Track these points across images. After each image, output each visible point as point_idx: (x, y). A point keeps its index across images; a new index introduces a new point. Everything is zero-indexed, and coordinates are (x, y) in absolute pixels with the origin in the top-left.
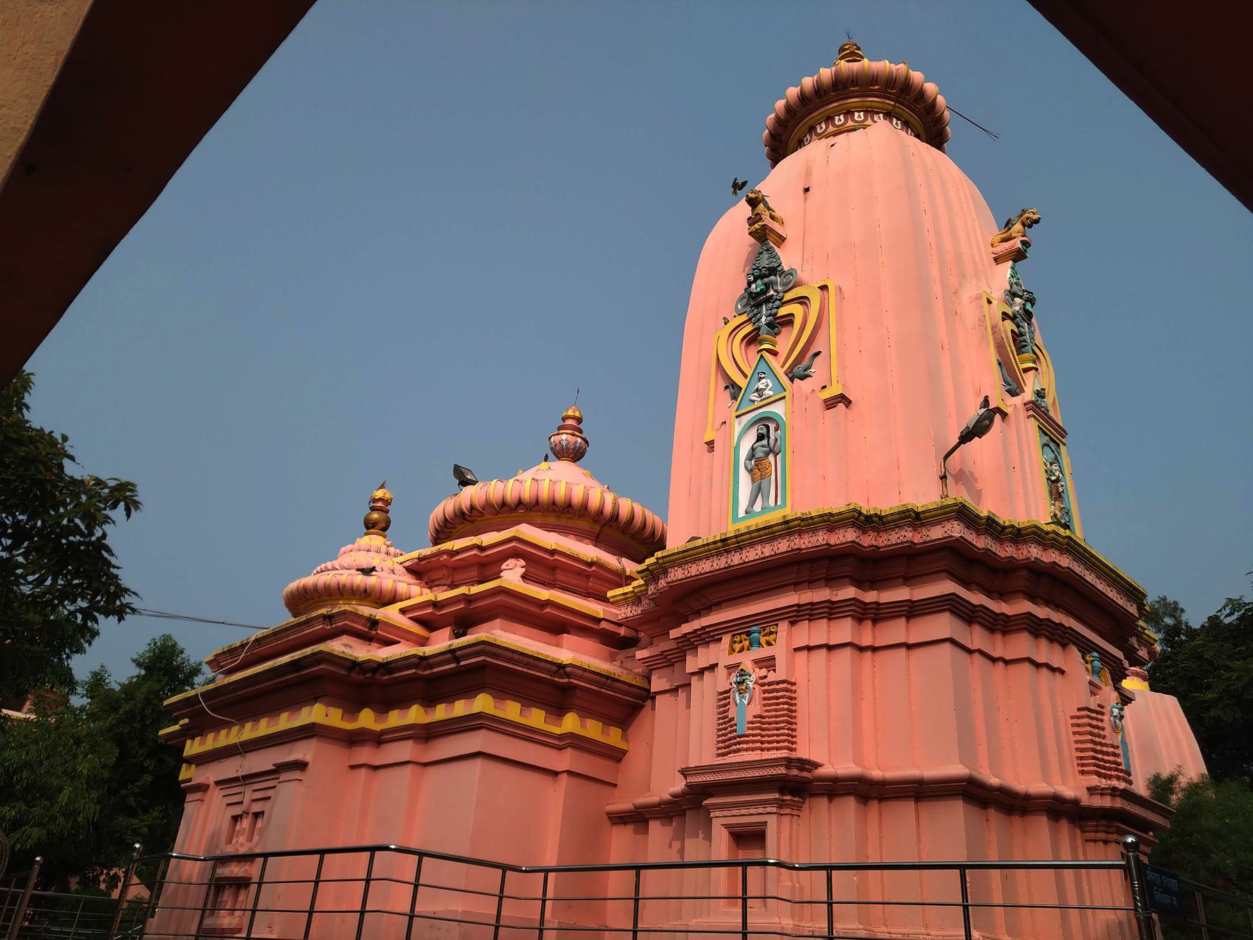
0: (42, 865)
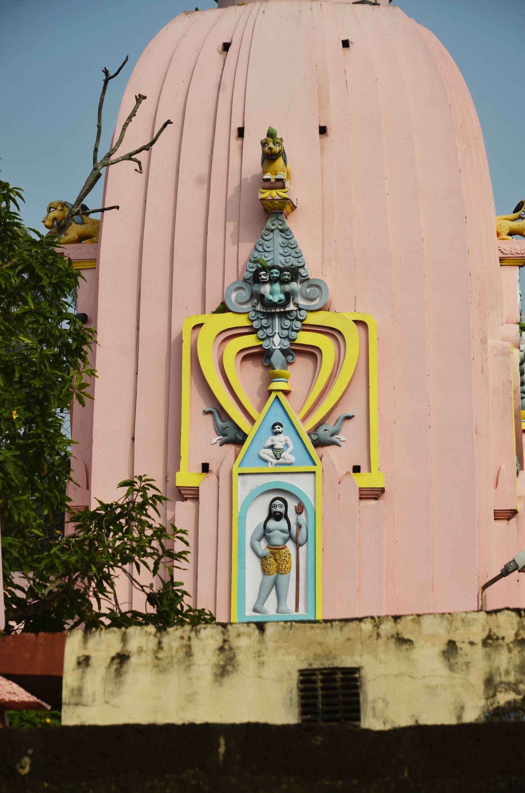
0: (37, 554)
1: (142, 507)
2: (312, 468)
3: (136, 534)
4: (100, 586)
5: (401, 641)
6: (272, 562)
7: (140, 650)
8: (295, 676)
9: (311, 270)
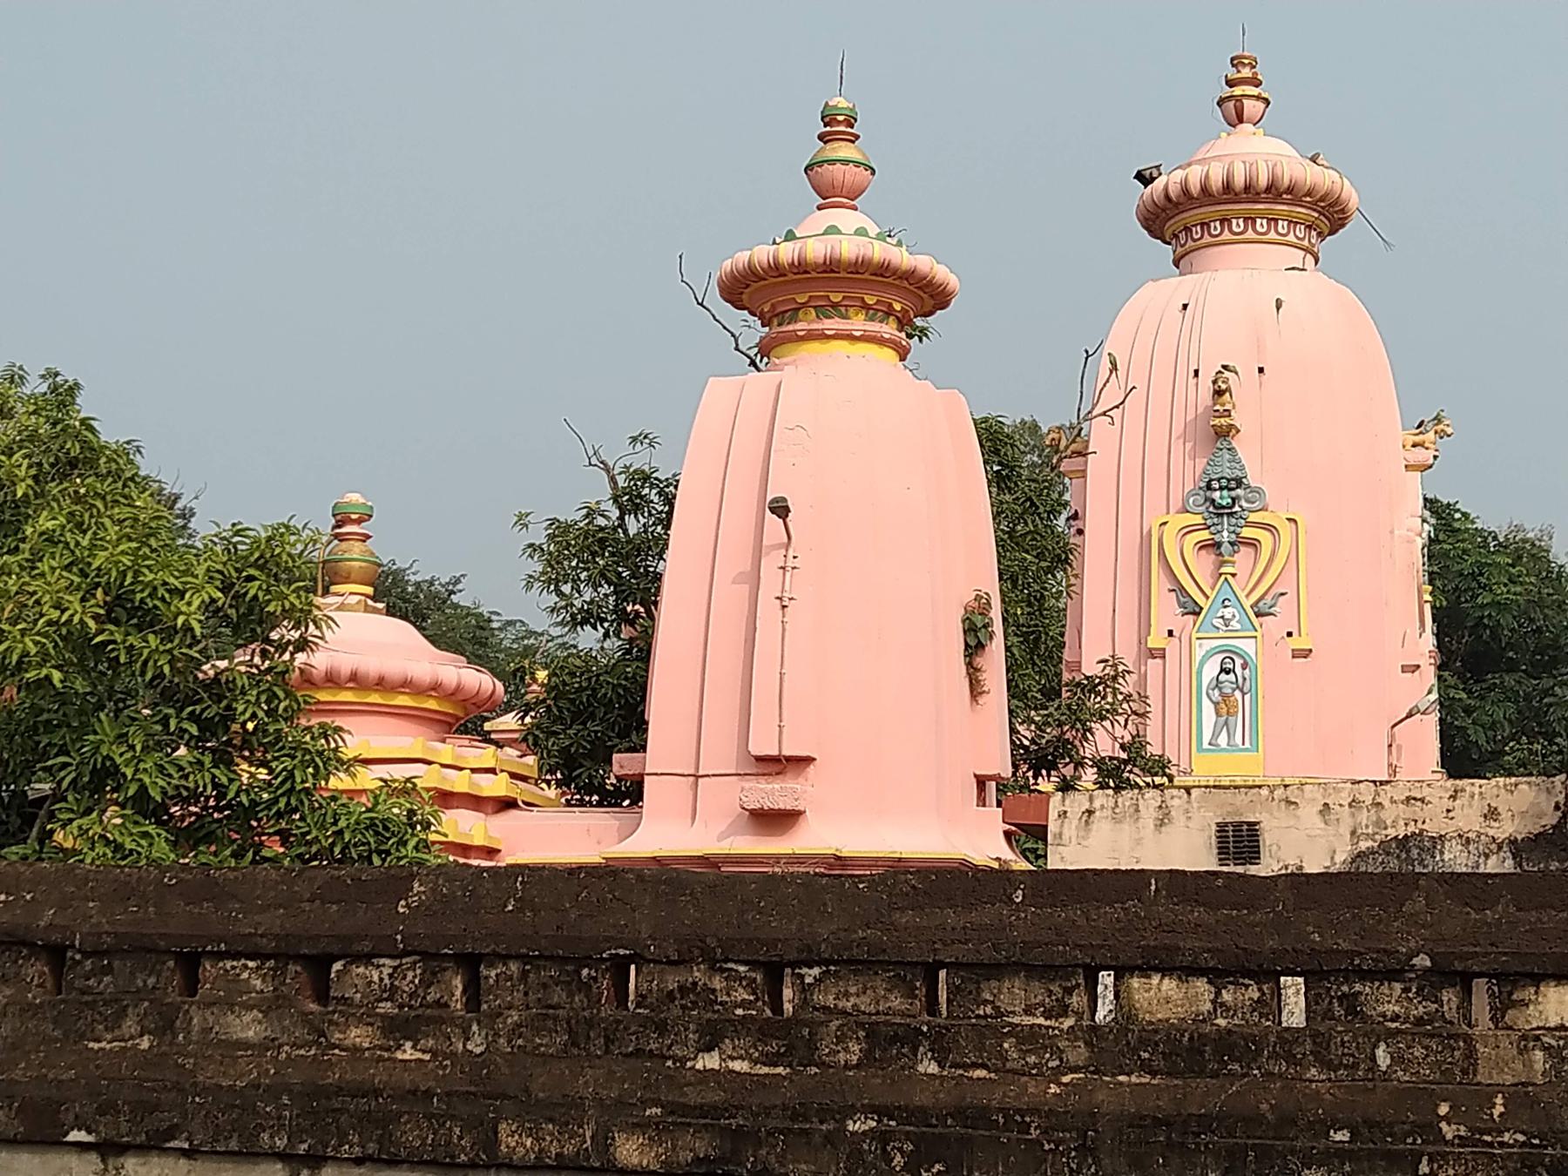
1: (1115, 678)
3: (1110, 699)
4: (1084, 735)
6: (1225, 707)
7: (1102, 807)
9: (1251, 481)
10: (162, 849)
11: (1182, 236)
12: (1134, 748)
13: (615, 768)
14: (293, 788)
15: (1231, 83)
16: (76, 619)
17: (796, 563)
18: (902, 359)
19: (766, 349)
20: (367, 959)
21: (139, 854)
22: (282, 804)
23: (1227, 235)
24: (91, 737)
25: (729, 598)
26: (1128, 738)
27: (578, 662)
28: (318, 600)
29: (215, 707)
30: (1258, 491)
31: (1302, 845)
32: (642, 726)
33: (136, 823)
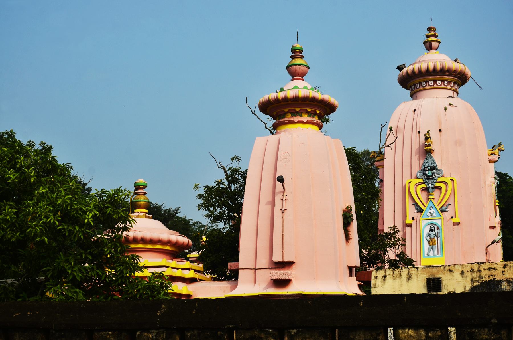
1: (394, 233)
2: (440, 218)
3: (393, 240)
5: (451, 271)
6: (431, 242)
7: (389, 275)
8: (426, 280)
9: (439, 167)
10: (81, 297)
11: (413, 87)
12: (402, 256)
13: (229, 267)
14: (123, 275)
15: (428, 36)
16: (52, 221)
17: (287, 197)
18: (320, 129)
19: (275, 127)
20: (148, 330)
21: (73, 298)
22: (120, 281)
23: (428, 87)
24: (57, 260)
25: (265, 210)
26: (399, 253)
27: (216, 233)
28: (130, 214)
29: (97, 250)
30: (440, 171)
31: (455, 284)
32: (238, 253)
33: (72, 288)
